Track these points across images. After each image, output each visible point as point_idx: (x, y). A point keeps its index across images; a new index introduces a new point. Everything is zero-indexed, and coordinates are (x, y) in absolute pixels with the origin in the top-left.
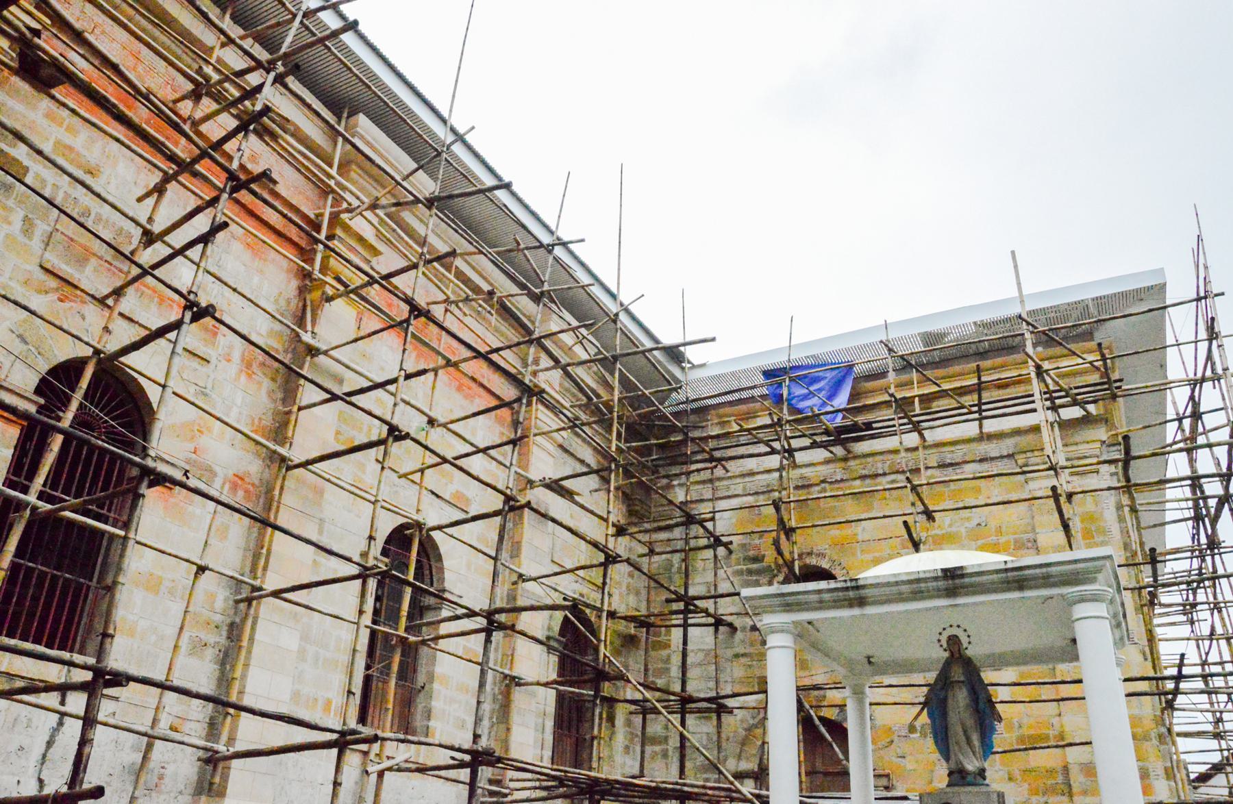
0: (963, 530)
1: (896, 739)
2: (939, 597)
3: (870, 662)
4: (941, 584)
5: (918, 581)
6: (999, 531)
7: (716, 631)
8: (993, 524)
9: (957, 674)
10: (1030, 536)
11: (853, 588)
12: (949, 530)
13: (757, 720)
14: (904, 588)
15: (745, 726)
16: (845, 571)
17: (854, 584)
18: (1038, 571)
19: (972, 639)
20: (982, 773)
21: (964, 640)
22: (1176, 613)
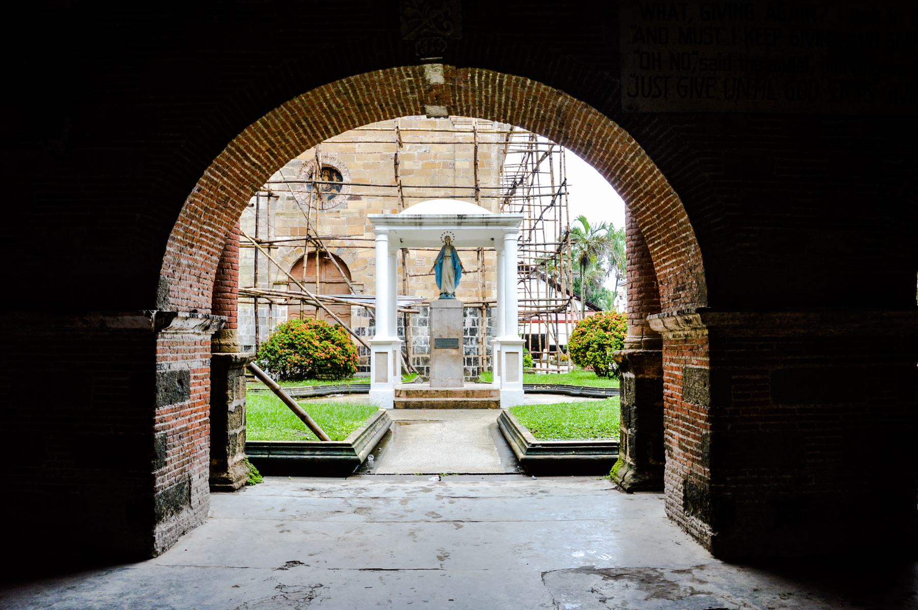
0: (416, 153)
1: (368, 266)
2: (455, 225)
3: (401, 242)
4: (456, 221)
5: (447, 218)
6: (435, 157)
7: (269, 198)
8: (433, 152)
9: (448, 252)
10: (452, 161)
11: (418, 218)
12: (408, 152)
13: (289, 252)
14: (442, 220)
15: (282, 255)
16: (346, 169)
17: (419, 217)
18: (495, 219)
19: (454, 235)
20: (454, 294)
21: (452, 239)
22: (694, 437)
